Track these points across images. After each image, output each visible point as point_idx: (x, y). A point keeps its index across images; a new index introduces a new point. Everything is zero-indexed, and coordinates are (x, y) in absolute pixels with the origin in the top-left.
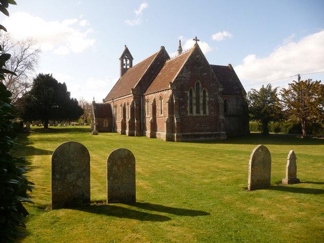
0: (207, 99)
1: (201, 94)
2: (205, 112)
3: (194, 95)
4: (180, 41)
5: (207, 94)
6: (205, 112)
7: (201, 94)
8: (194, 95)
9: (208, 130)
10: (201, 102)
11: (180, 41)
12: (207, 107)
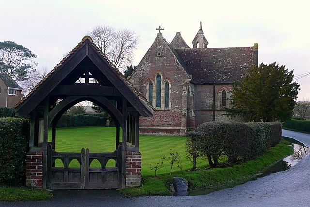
0: (170, 91)
1: (163, 86)
2: (167, 105)
3: (154, 88)
4: (201, 23)
5: (170, 86)
6: (167, 105)
7: (163, 86)
8: (154, 88)
9: (170, 125)
10: (163, 94)
11: (201, 23)
12: (170, 100)
